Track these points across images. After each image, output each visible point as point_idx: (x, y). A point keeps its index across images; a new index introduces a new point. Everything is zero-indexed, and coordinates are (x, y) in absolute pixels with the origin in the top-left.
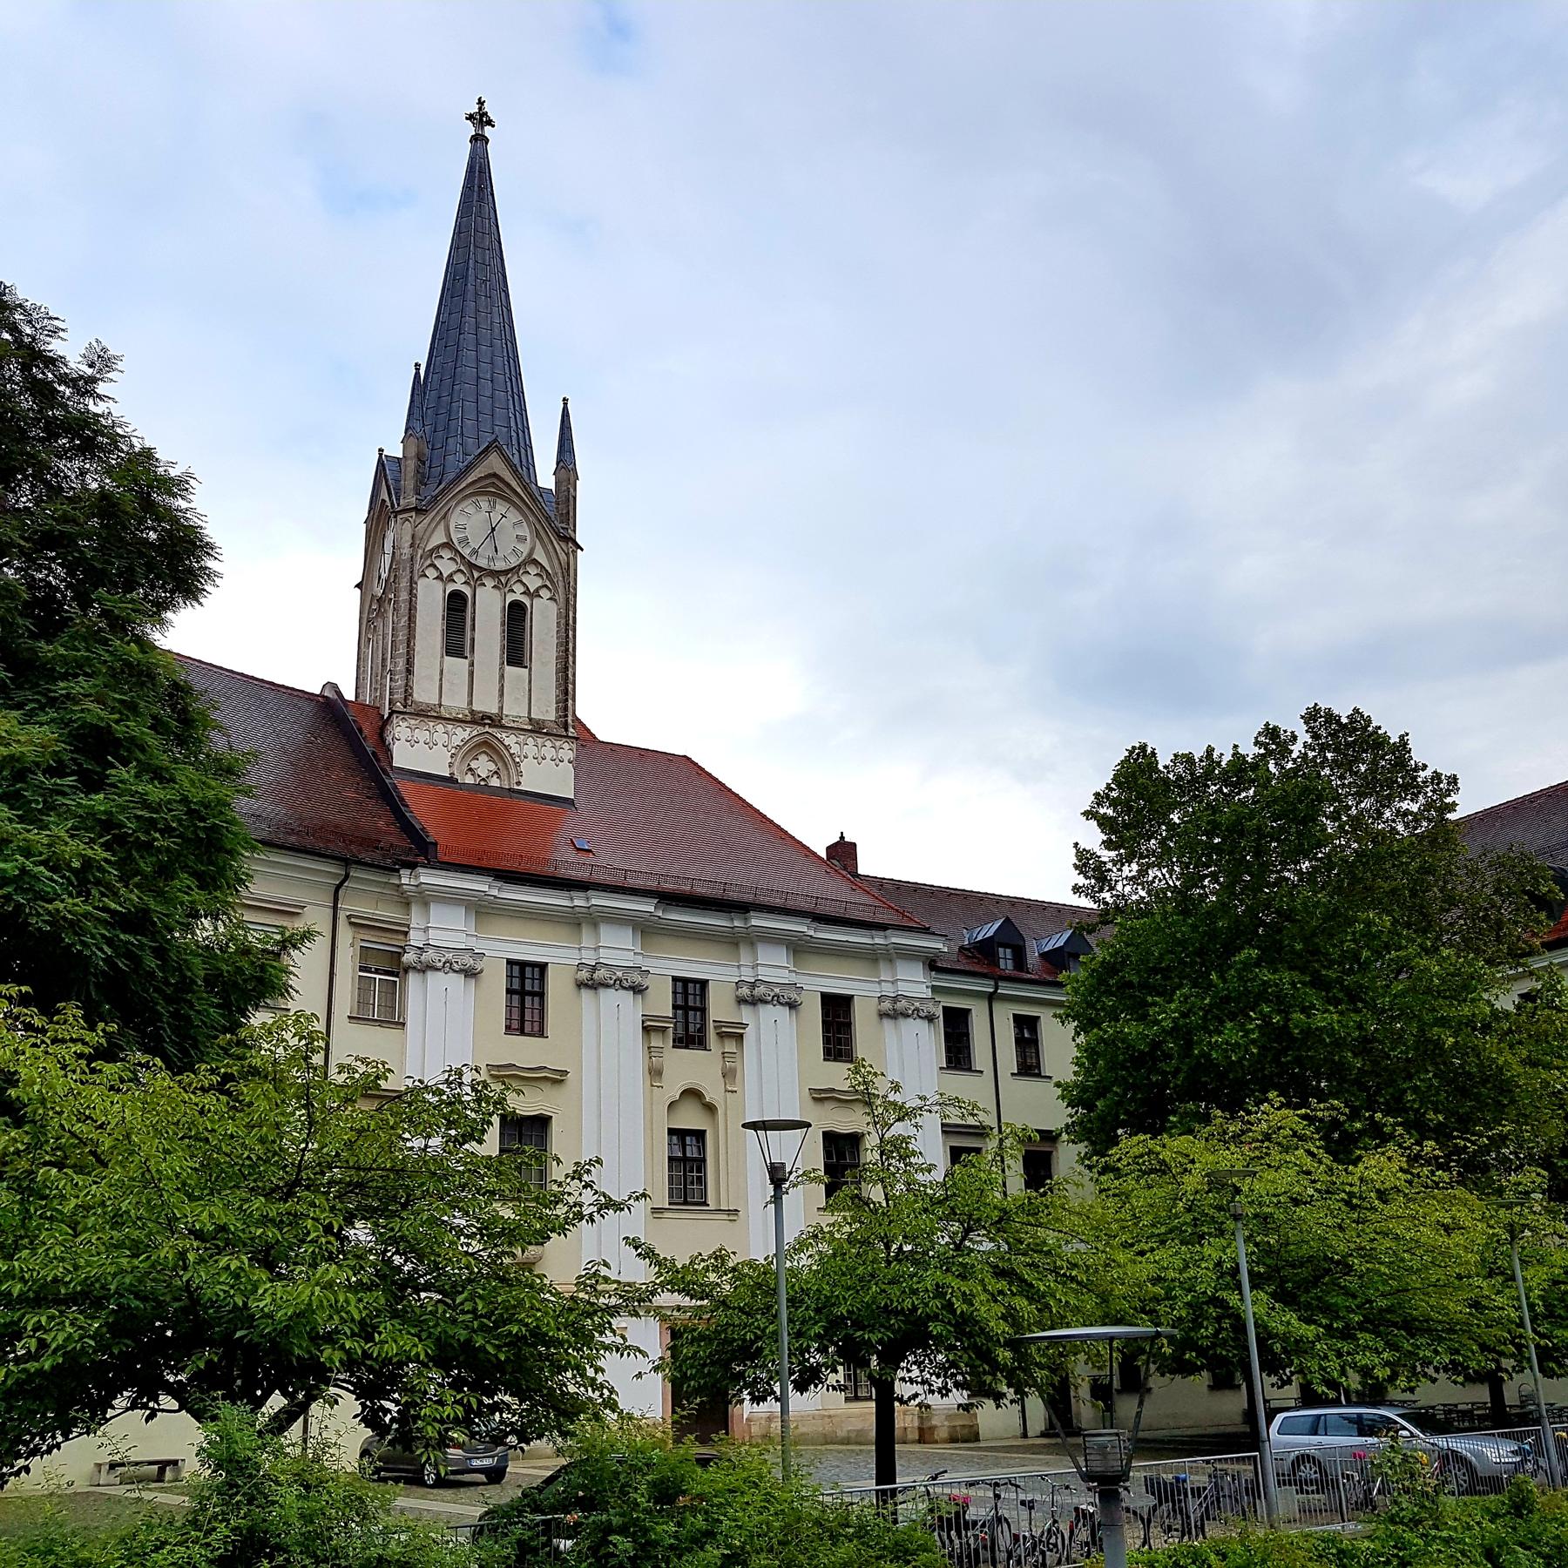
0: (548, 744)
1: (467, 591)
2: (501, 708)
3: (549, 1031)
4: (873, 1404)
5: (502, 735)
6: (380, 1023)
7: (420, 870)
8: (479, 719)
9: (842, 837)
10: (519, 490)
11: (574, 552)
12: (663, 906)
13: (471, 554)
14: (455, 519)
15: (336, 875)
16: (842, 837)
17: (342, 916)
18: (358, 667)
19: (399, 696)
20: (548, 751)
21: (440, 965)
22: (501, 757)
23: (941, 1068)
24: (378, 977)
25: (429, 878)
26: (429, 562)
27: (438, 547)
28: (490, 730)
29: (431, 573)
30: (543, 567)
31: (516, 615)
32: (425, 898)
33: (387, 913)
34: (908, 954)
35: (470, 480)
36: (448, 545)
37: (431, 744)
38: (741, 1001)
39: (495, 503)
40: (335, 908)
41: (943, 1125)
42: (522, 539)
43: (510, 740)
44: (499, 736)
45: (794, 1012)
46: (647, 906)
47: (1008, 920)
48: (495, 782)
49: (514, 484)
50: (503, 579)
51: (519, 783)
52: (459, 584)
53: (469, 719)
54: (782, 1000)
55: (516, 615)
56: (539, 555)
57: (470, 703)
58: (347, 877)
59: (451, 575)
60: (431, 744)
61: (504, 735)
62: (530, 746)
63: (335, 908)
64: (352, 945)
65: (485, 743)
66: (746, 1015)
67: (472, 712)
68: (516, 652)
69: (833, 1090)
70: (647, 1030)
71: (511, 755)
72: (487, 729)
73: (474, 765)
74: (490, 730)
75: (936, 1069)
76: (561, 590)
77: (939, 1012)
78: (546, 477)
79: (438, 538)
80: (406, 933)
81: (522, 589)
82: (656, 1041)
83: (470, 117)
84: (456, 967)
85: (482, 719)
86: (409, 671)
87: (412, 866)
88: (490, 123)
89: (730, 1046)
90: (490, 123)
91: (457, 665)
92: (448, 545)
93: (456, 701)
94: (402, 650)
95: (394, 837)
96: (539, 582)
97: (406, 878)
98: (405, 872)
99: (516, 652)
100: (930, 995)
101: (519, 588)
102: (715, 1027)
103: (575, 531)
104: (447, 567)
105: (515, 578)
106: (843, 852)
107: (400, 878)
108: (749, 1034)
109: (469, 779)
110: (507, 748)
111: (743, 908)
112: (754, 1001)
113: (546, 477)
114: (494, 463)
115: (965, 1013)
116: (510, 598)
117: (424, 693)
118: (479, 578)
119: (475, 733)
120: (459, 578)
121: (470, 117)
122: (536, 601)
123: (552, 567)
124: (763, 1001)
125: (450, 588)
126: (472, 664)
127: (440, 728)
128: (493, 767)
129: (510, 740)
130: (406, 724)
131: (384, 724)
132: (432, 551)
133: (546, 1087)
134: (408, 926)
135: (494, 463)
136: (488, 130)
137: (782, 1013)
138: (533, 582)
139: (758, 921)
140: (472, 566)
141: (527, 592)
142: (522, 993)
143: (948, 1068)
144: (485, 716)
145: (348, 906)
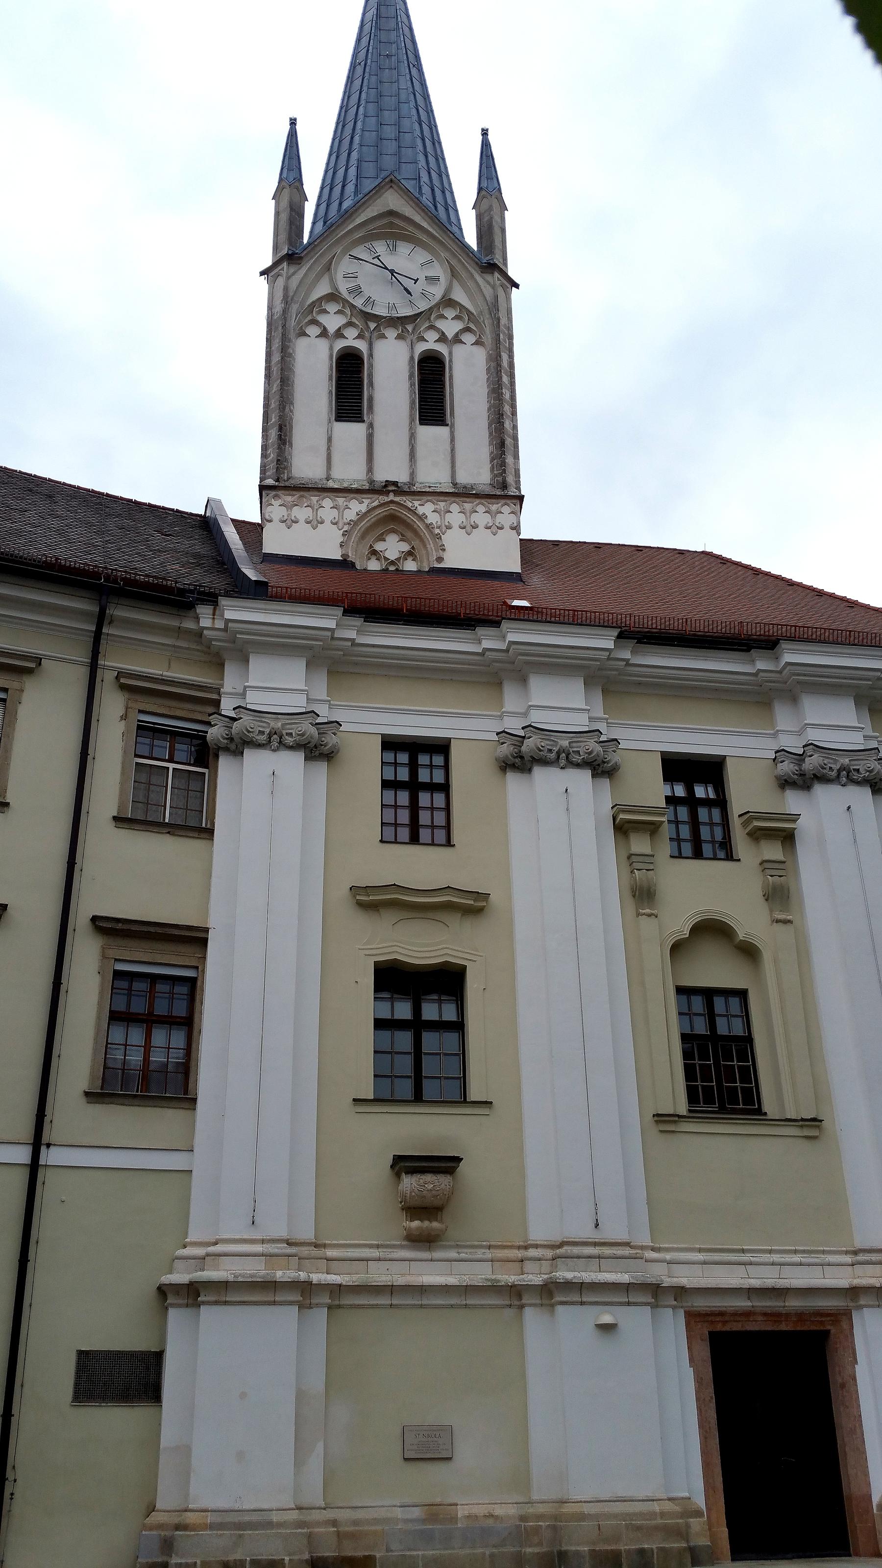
0: (481, 509)
1: (362, 346)
2: (412, 474)
3: (456, 838)
4: (390, 1018)
6: (173, 829)
7: (223, 601)
8: (389, 487)
10: (425, 225)
14: (345, 266)
17: (107, 678)
20: (481, 517)
21: (262, 738)
22: (416, 532)
24: (171, 766)
26: (310, 318)
27: (320, 299)
28: (397, 499)
29: (313, 331)
30: (462, 307)
35: (359, 221)
36: (333, 297)
38: (785, 783)
40: (93, 667)
42: (432, 280)
43: (427, 509)
44: (409, 505)
48: (410, 566)
49: (418, 218)
50: (410, 328)
51: (440, 559)
52: (351, 340)
54: (855, 776)
56: (459, 295)
57: (370, 470)
60: (315, 523)
61: (416, 503)
62: (456, 515)
63: (93, 667)
64: (124, 717)
65: (392, 518)
67: (371, 482)
70: (622, 829)
72: (391, 497)
73: (379, 547)
74: (397, 499)
76: (488, 330)
78: (471, 237)
79: (322, 289)
81: (436, 336)
82: (640, 844)
84: (289, 740)
85: (386, 486)
89: (773, 851)
92: (333, 297)
96: (458, 326)
98: (204, 611)
101: (432, 336)
102: (745, 824)
104: (332, 321)
107: (197, 619)
108: (805, 826)
109: (374, 565)
110: (422, 518)
113: (471, 237)
116: (421, 348)
119: (376, 503)
120: (351, 333)
123: (476, 306)
124: (820, 778)
125: (340, 344)
126: (371, 426)
127: (327, 503)
128: (405, 547)
129: (427, 509)
130: (280, 502)
132: (313, 304)
133: (454, 920)
135: (392, 200)
138: (450, 327)
141: (443, 338)
142: (414, 786)
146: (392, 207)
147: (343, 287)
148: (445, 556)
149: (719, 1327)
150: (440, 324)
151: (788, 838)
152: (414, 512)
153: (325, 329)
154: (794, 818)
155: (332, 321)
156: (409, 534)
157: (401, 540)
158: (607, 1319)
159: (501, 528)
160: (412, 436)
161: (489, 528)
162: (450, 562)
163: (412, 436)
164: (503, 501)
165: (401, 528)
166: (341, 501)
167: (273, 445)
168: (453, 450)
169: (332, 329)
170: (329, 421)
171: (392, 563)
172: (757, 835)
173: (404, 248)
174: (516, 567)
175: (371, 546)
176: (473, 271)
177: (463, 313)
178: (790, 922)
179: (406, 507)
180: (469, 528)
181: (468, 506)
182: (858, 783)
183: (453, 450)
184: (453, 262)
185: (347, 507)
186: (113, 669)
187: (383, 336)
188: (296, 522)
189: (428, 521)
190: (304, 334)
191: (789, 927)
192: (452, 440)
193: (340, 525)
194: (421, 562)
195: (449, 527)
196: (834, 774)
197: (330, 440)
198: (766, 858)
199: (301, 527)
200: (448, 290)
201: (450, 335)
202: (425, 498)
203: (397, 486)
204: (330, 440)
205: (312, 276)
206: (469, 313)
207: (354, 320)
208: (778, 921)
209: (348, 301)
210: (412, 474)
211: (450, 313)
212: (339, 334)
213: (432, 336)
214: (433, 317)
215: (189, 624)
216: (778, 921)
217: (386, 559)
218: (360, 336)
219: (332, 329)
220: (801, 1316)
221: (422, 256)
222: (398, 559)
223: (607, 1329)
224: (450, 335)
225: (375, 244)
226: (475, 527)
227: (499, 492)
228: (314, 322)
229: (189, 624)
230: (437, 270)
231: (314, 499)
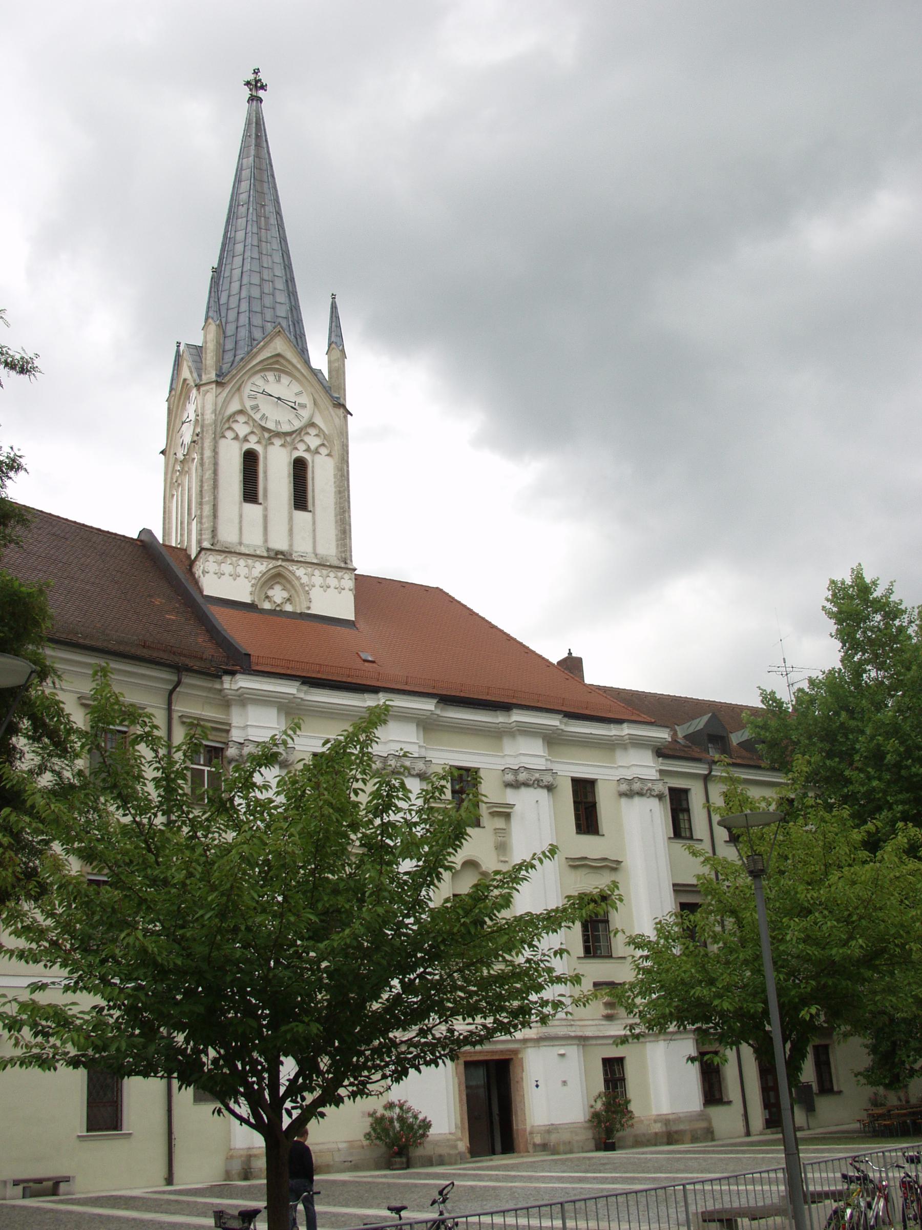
0: (332, 575)
1: (259, 448)
2: (291, 545)
5: (293, 568)
8: (276, 555)
9: (570, 653)
10: (299, 366)
11: (345, 417)
12: (441, 705)
13: (261, 419)
15: (171, 681)
16: (570, 653)
17: (175, 716)
18: (164, 518)
19: (207, 535)
20: (332, 581)
22: (293, 586)
23: (670, 838)
24: (206, 769)
25: (244, 683)
26: (227, 426)
29: (229, 434)
30: (320, 429)
31: (300, 468)
32: (244, 700)
33: (210, 713)
34: (637, 743)
37: (235, 576)
38: (508, 785)
39: (280, 377)
41: (674, 885)
43: (300, 572)
45: (551, 794)
46: (428, 705)
47: (713, 714)
48: (288, 608)
50: (288, 439)
51: (309, 608)
52: (252, 445)
53: (265, 554)
55: (300, 468)
56: (318, 420)
58: (178, 683)
59: (246, 436)
60: (235, 576)
61: (295, 568)
62: (317, 578)
66: (511, 796)
67: (268, 550)
68: (300, 500)
69: (586, 858)
71: (302, 585)
72: (280, 563)
73: (270, 593)
74: (284, 564)
75: (666, 838)
77: (667, 792)
78: (319, 359)
79: (234, 406)
80: (228, 731)
83: (248, 83)
86: (215, 516)
87: (232, 673)
88: (263, 87)
89: (500, 823)
90: (263, 87)
91: (251, 509)
93: (253, 539)
94: (207, 498)
95: (209, 650)
97: (228, 684)
98: (226, 679)
99: (300, 500)
100: (658, 777)
103: (345, 399)
104: (242, 429)
105: (298, 439)
106: (572, 665)
107: (222, 683)
108: (517, 811)
109: (267, 606)
110: (299, 578)
111: (506, 707)
112: (515, 785)
114: (279, 346)
115: (686, 792)
116: (296, 454)
117: (228, 535)
118: (270, 439)
119: (271, 566)
121: (248, 83)
122: (317, 457)
125: (246, 446)
126: (266, 509)
127: (242, 562)
128: (285, 595)
131: (192, 563)
134: (230, 725)
136: (261, 93)
137: (544, 793)
139: (518, 717)
140: (264, 429)
141: (308, 450)
143: (585, 957)
144: (278, 553)
145: (179, 708)
146: (279, 351)
147: (248, 404)
148: (312, 605)
149: (469, 1059)
150: (307, 439)
151: (507, 816)
152: (294, 574)
153: (237, 435)
154: (512, 806)
155: (242, 429)
156: (288, 586)
157: (283, 589)
158: (562, 1052)
159: (344, 589)
160: (291, 519)
161: (337, 588)
162: (316, 610)
163: (291, 519)
164: (344, 571)
165: (283, 581)
166: (250, 562)
167: (208, 517)
168: (314, 530)
169: (241, 435)
170: (241, 504)
171: (278, 605)
172: (493, 814)
173: (285, 380)
174: (351, 617)
175: (266, 593)
176: (328, 406)
177: (320, 433)
178: (507, 862)
179: (289, 570)
180: (325, 588)
181: (325, 572)
182: (541, 787)
183: (314, 530)
184: (316, 396)
185: (254, 567)
186: (178, 711)
187: (272, 444)
188: (224, 574)
189: (302, 581)
190: (224, 437)
191: (506, 864)
192: (314, 523)
193: (250, 578)
194: (296, 606)
195: (313, 586)
196: (531, 782)
197: (241, 516)
198: (498, 827)
199: (226, 578)
200: (312, 416)
201: (313, 447)
202: (300, 565)
203: (284, 555)
204: (241, 516)
205: (230, 395)
206: (324, 434)
207: (255, 430)
208: (502, 861)
209: (251, 417)
210: (291, 545)
211: (313, 431)
212: (245, 439)
213: (302, 447)
214: (303, 433)
215: (218, 686)
216: (502, 861)
217: (275, 602)
218: (258, 442)
219: (241, 435)
220: (502, 1052)
221: (296, 387)
222: (282, 603)
223: (562, 1055)
224: (313, 447)
225: (267, 373)
226: (328, 587)
227: (343, 565)
228: (230, 428)
229: (218, 686)
230: (304, 399)
231: (234, 559)
